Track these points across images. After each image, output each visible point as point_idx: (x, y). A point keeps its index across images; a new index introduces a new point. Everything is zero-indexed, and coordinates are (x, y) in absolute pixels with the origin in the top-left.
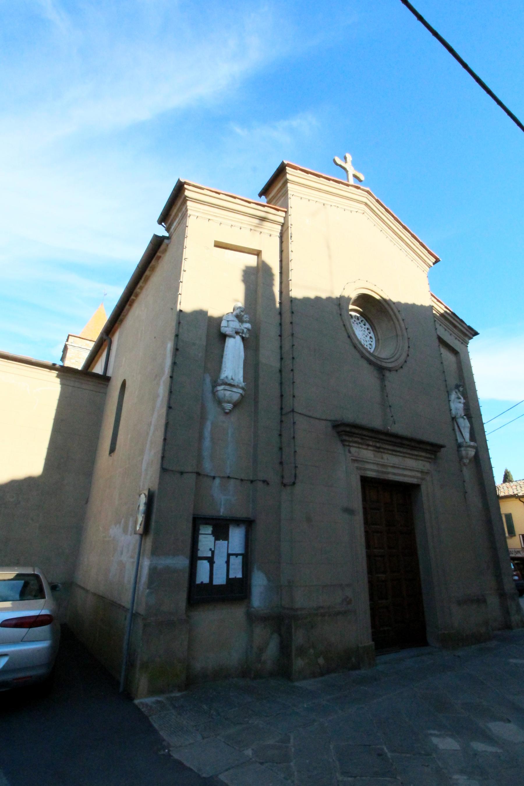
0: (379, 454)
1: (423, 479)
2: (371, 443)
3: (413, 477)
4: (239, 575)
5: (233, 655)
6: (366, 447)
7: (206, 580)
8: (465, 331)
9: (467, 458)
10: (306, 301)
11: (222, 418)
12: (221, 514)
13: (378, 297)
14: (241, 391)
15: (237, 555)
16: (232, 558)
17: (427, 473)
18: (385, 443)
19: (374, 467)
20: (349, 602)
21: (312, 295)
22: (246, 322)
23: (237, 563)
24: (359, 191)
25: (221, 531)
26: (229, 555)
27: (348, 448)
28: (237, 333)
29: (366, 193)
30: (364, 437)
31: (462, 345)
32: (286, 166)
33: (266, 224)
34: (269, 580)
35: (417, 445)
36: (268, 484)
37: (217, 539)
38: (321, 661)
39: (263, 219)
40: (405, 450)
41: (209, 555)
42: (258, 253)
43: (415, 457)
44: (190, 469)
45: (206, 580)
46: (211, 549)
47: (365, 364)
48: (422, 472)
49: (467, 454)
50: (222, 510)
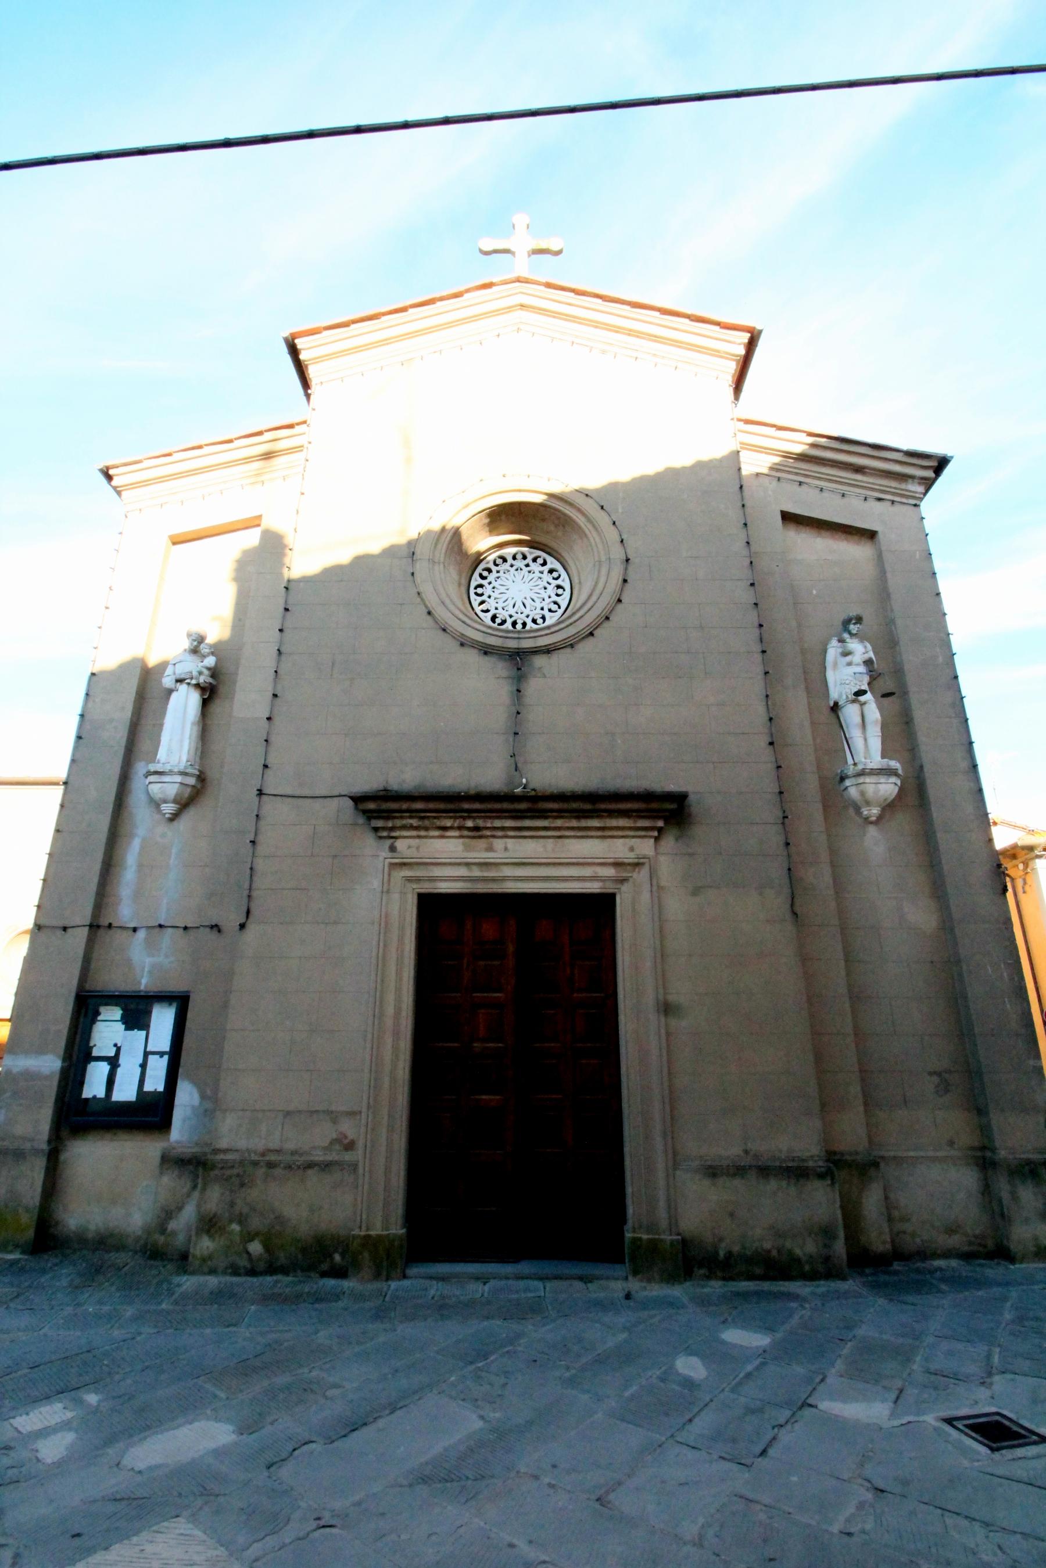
0: (482, 843)
1: (623, 881)
2: (448, 823)
3: (594, 878)
4: (161, 1088)
5: (134, 1217)
6: (437, 833)
7: (101, 1093)
8: (897, 468)
9: (868, 803)
10: (333, 575)
11: (162, 829)
12: (142, 988)
13: (538, 499)
14: (178, 779)
15: (161, 1054)
16: (152, 1059)
17: (637, 865)
18: (490, 818)
19: (463, 872)
20: (350, 1146)
21: (344, 557)
22: (208, 655)
23: (158, 1068)
24: (494, 288)
25: (136, 1016)
26: (146, 1054)
27: (389, 842)
28: (180, 681)
29: (517, 284)
30: (423, 815)
31: (897, 508)
32: (293, 340)
33: (276, 461)
34: (203, 1097)
35: (588, 806)
36: (219, 931)
37: (129, 1028)
38: (256, 1248)
39: (268, 456)
40: (559, 823)
41: (112, 1053)
42: (253, 523)
43: (599, 833)
44: (78, 921)
45: (101, 1093)
46: (115, 1045)
47: (472, 656)
48: (617, 865)
49: (862, 794)
50: (144, 981)
